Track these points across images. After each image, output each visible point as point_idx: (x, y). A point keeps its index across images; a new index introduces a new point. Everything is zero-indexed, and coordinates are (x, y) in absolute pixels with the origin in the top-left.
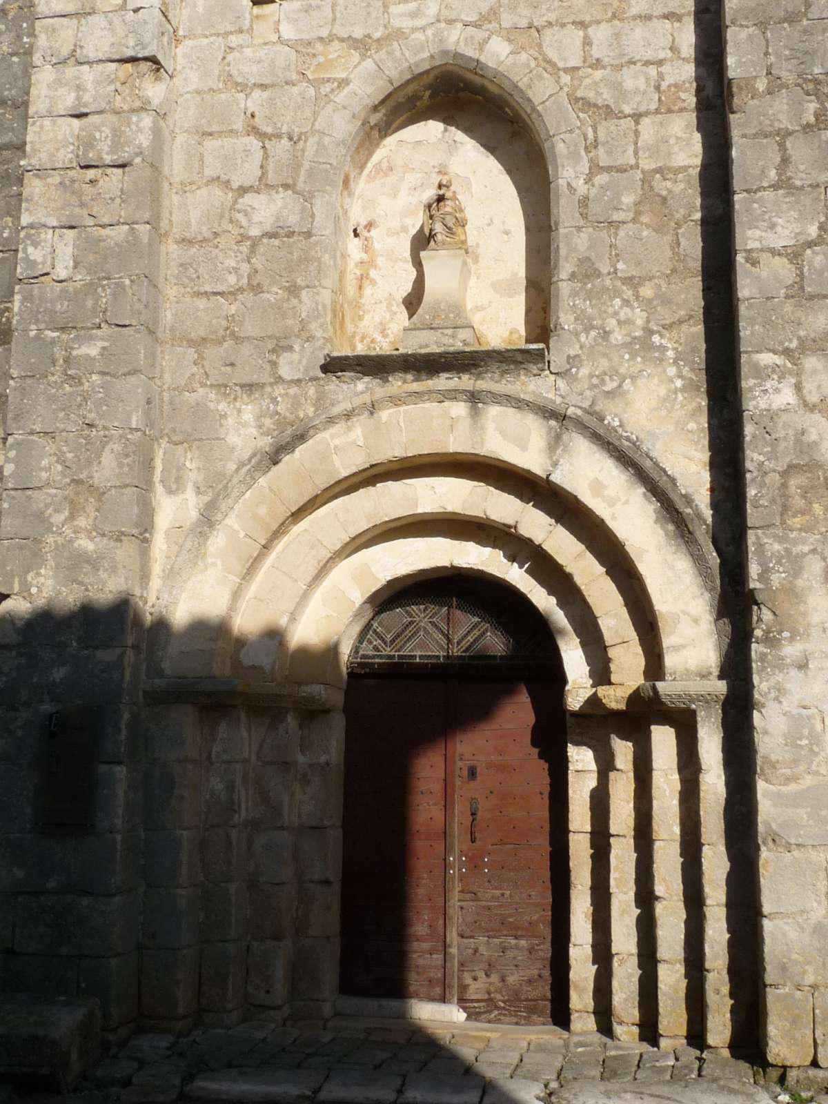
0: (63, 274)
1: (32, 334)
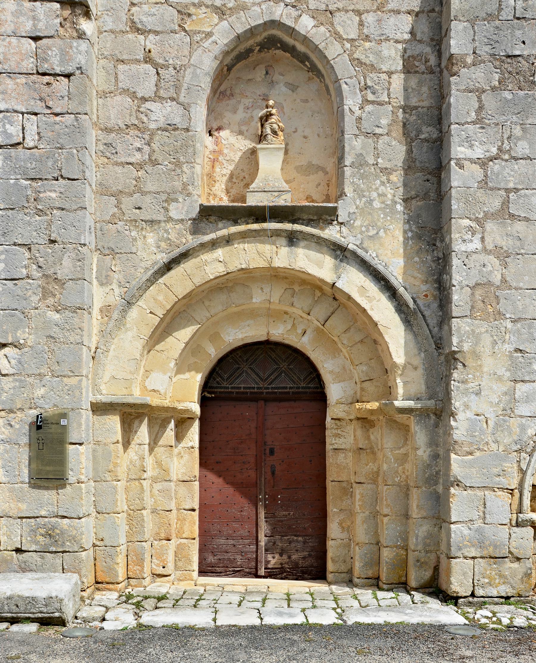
0: (31, 144)
1: (12, 181)
